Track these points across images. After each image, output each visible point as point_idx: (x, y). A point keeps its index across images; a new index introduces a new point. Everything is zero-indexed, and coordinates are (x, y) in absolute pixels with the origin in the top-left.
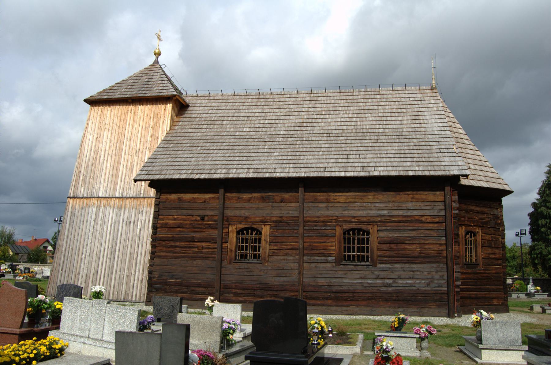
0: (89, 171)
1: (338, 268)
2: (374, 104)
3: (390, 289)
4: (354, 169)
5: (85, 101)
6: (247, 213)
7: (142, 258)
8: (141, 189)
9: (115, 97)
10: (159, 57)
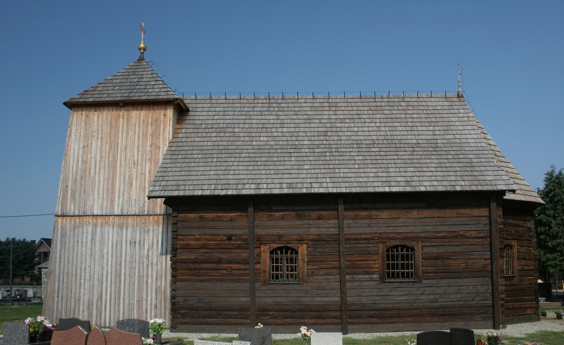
0: (78, 186)
1: (382, 286)
2: (400, 112)
3: (436, 304)
4: (397, 184)
5: (65, 104)
6: (280, 232)
7: (154, 282)
8: (144, 205)
9: (103, 99)
10: (145, 53)
